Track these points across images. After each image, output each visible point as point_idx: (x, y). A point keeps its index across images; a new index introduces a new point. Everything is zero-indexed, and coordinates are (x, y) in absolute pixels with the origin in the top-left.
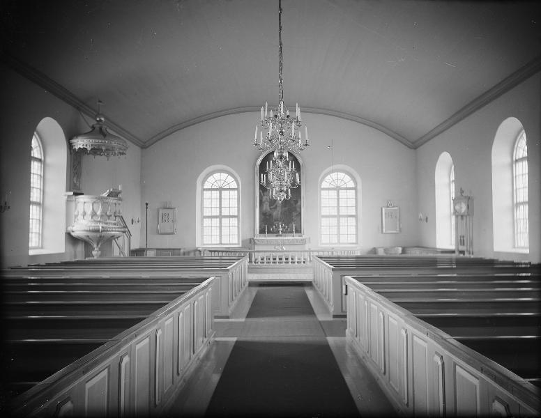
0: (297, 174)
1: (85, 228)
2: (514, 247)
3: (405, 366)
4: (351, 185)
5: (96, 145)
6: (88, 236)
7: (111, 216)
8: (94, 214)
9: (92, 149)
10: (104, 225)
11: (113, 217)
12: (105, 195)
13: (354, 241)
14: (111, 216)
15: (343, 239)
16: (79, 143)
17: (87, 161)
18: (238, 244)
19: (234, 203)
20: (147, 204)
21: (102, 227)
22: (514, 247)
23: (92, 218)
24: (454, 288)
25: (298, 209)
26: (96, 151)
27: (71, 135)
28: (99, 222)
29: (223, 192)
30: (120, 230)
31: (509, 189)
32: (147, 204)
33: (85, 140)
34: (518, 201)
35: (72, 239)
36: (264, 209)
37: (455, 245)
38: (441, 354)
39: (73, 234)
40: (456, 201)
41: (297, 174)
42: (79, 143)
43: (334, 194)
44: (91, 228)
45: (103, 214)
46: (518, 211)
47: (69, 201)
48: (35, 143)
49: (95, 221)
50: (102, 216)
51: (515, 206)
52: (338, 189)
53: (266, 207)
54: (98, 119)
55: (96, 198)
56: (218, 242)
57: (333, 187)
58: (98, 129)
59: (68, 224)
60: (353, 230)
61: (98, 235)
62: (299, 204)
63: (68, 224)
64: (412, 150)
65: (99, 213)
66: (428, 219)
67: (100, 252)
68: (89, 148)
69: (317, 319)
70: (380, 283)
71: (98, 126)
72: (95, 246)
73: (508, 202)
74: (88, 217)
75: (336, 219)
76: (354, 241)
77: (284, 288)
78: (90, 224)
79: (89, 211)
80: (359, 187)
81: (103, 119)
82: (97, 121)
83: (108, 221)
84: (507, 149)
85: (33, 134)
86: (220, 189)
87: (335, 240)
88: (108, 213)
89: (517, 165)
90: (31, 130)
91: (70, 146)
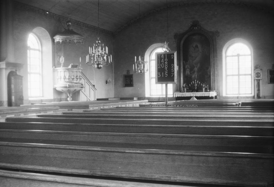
0: (109, 57)
1: (63, 86)
2: (226, 94)
3: (9, 165)
5: (64, 39)
6: (63, 90)
7: (74, 78)
8: (65, 78)
10: (70, 84)
11: (75, 79)
14: (74, 78)
18: (252, 94)
21: (69, 85)
23: (64, 80)
24: (134, 119)
25: (209, 73)
35: (59, 93)
36: (186, 73)
37: (225, 97)
41: (109, 57)
45: (69, 77)
47: (54, 71)
50: (69, 79)
53: (188, 72)
54: (68, 24)
56: (41, 96)
59: (54, 84)
62: (209, 69)
63: (54, 84)
65: (67, 77)
66: (105, 82)
67: (71, 99)
68: (61, 41)
70: (120, 119)
74: (63, 80)
79: (63, 77)
81: (70, 24)
83: (73, 81)
88: (72, 77)
91: (53, 40)
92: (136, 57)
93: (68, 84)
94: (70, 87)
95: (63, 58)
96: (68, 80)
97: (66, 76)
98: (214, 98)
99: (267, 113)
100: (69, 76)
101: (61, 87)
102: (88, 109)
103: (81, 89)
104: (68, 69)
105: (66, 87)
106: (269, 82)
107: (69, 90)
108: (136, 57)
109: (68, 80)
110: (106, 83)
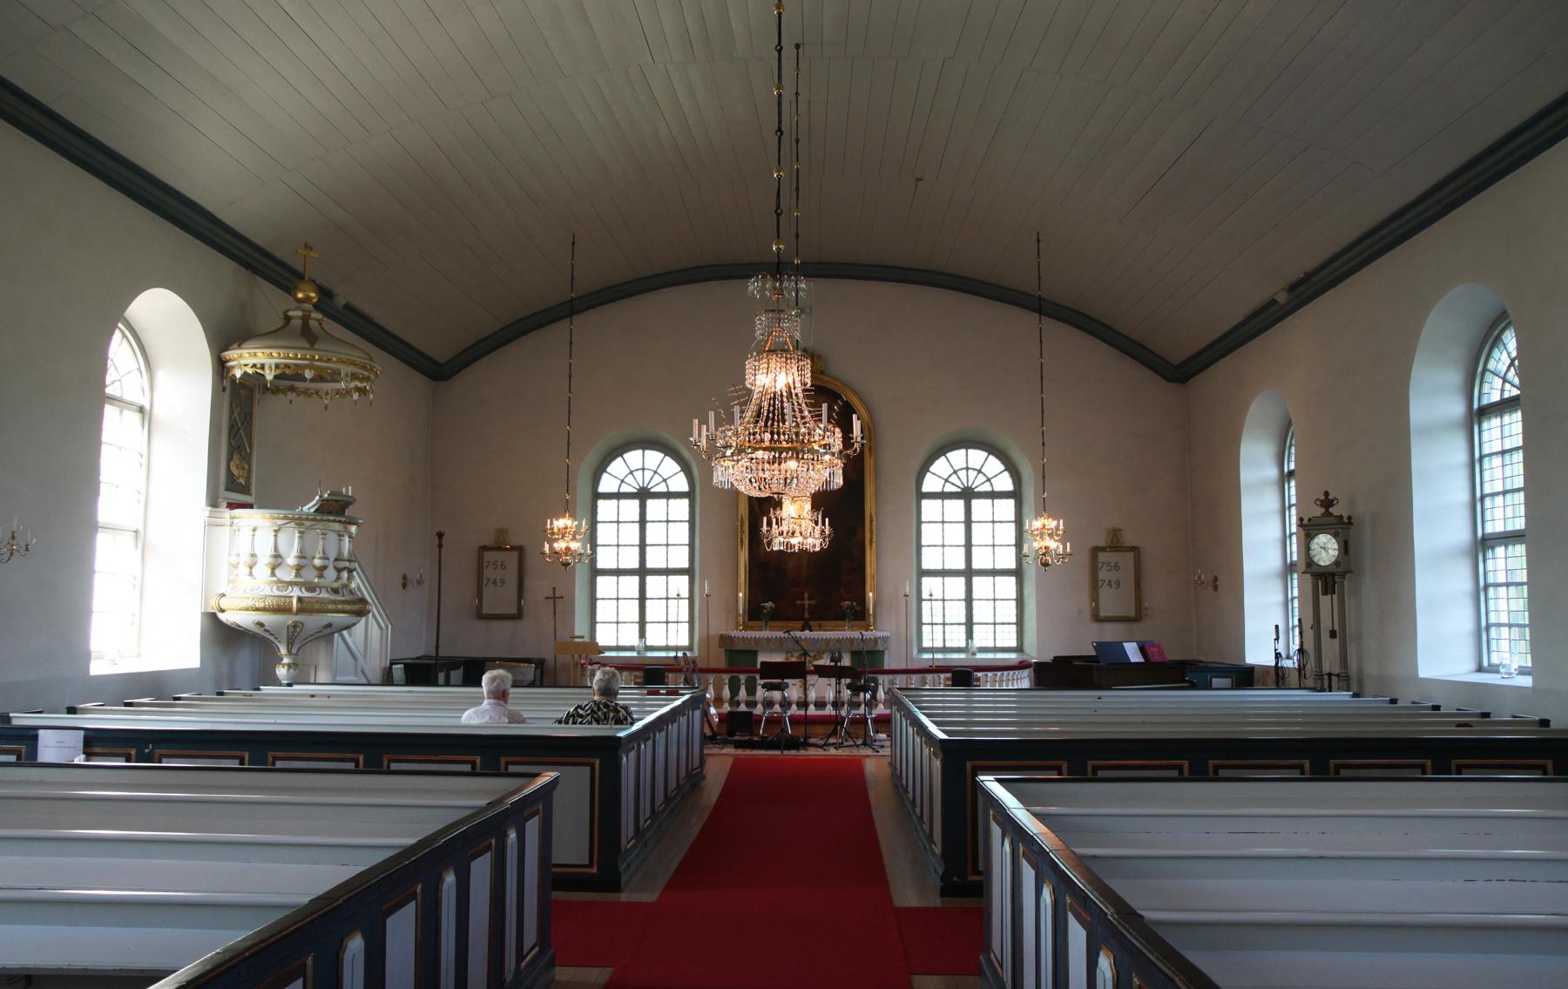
4: (1005, 483)
5: (287, 366)
6: (261, 625)
8: (277, 559)
9: (276, 377)
10: (306, 594)
12: (310, 507)
13: (1013, 644)
14: (324, 568)
15: (982, 637)
16: (247, 359)
17: (270, 415)
19: (681, 533)
20: (440, 535)
21: (300, 599)
22: (1480, 669)
26: (288, 378)
27: (224, 337)
28: (291, 583)
29: (650, 502)
30: (348, 607)
31: (1461, 495)
32: (440, 535)
33: (259, 353)
34: (1489, 529)
38: (273, 533)
39: (222, 616)
40: (1309, 529)
42: (247, 359)
43: (956, 508)
44: (268, 602)
45: (304, 562)
46: (1490, 563)
48: (120, 351)
49: (280, 581)
51: (1483, 544)
52: (967, 495)
54: (300, 295)
55: (285, 518)
57: (955, 489)
58: (299, 322)
60: (1009, 612)
61: (289, 619)
64: (418, 381)
65: (291, 560)
69: (513, 677)
71: (299, 313)
72: (283, 650)
73: (1459, 533)
74: (263, 570)
75: (976, 580)
76: (1013, 644)
77: (437, 608)
78: (267, 591)
79: (265, 558)
80: (1029, 493)
82: (299, 301)
84: (1453, 377)
85: (116, 327)
86: (643, 495)
87: (957, 638)
88: (317, 562)
89: (1485, 425)
90: (111, 314)
91: (221, 367)
92: (549, 521)
93: (296, 593)
94: (305, 607)
95: (906, 722)
96: (289, 576)
97: (282, 550)
98: (1293, 678)
99: (131, 334)
100: (302, 556)
101: (257, 609)
102: (1322, 594)
103: (353, 619)
104: (299, 521)
105: (281, 609)
106: (863, 622)
107: (295, 625)
108: (549, 521)
109: (289, 576)
110: (404, 586)
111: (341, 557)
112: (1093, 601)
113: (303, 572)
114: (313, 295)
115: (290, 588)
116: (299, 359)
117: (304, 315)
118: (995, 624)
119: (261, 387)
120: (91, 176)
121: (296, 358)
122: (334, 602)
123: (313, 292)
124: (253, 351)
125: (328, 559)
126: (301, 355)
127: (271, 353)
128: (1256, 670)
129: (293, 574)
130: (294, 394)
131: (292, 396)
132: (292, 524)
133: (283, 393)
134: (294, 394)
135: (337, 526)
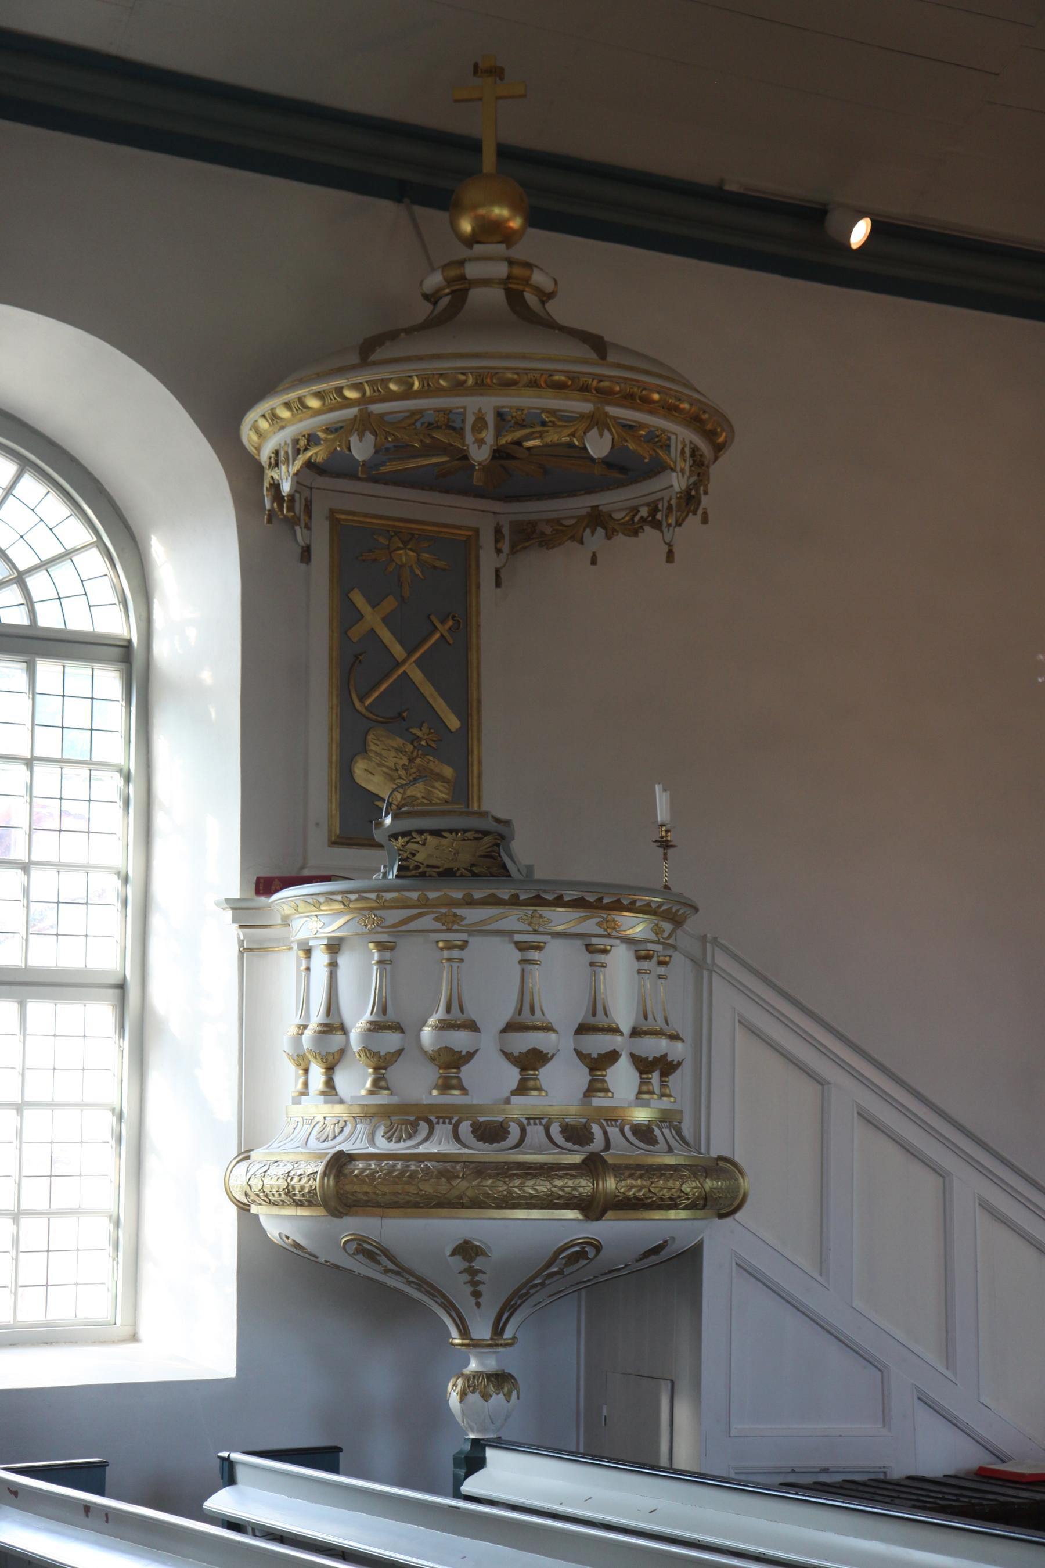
45: (391, 1041)
111: (601, 1020)
112: (581, 415)
113: (393, 1074)
114: (500, 212)
115: (424, 1128)
116: (418, 395)
117: (510, 277)
118: (58, 903)
119: (506, 530)
120: (113, 50)
121: (408, 394)
122: (481, 1170)
123: (499, 203)
124: (292, 395)
125: (472, 1026)
126: (422, 379)
127: (301, 400)
128: (452, 1495)
129: (368, 1084)
130: (600, 531)
131: (596, 540)
132: (427, 922)
133: (572, 538)
134: (600, 531)
135: (513, 919)
